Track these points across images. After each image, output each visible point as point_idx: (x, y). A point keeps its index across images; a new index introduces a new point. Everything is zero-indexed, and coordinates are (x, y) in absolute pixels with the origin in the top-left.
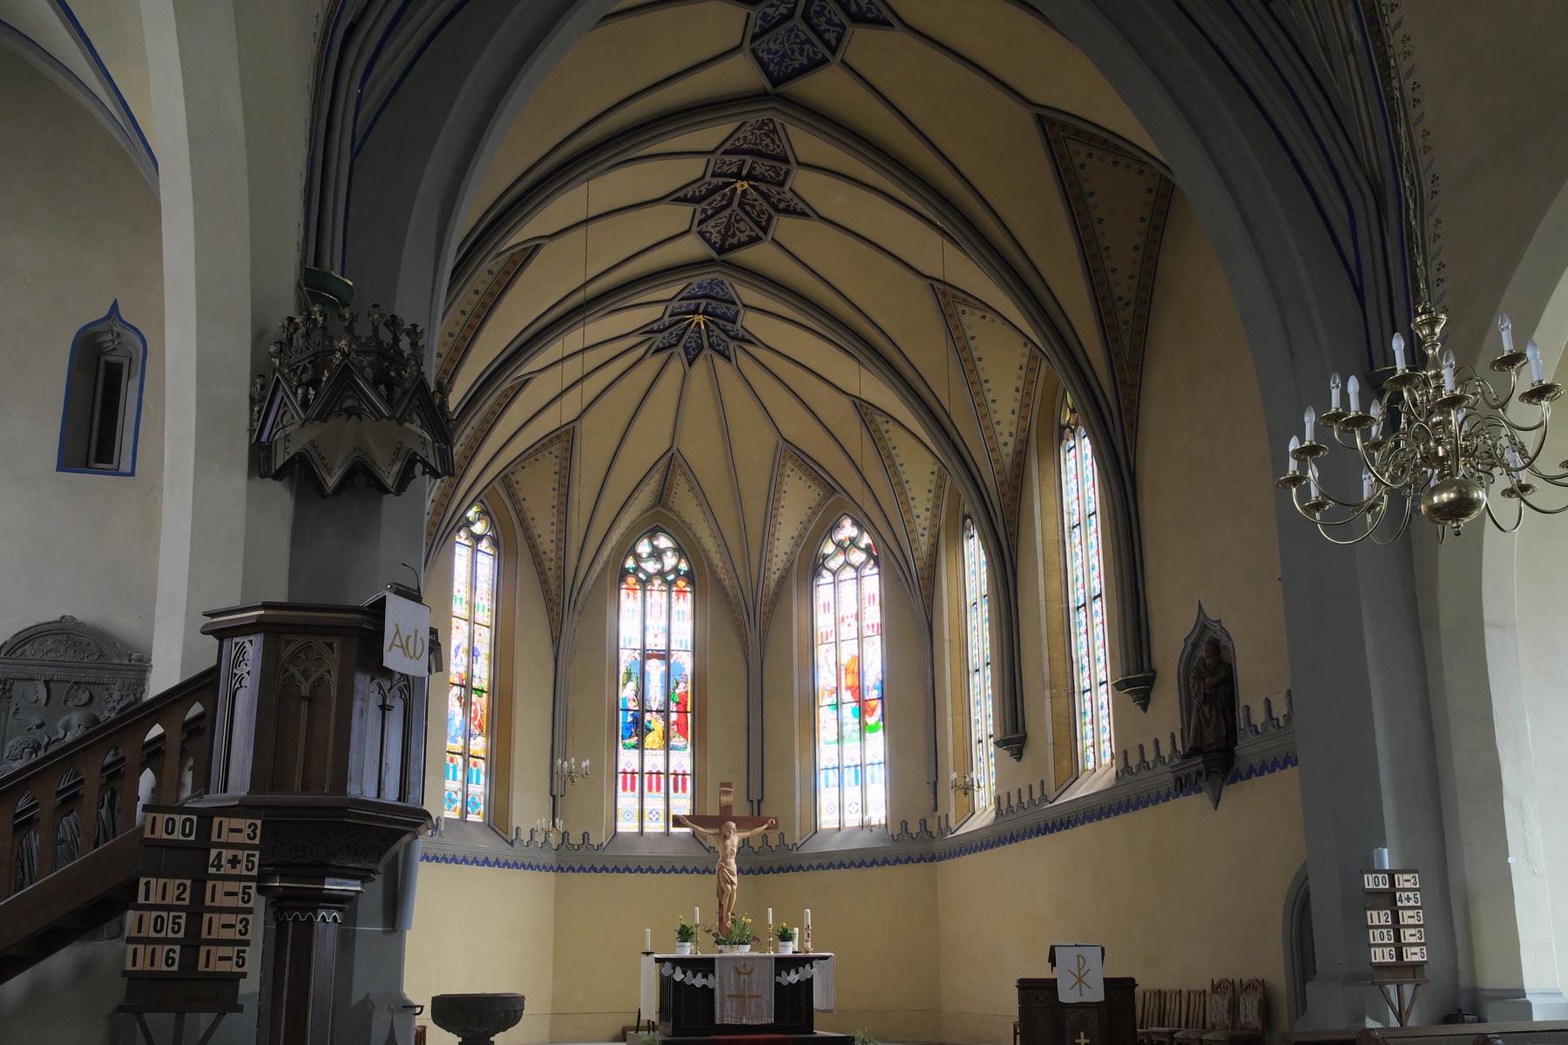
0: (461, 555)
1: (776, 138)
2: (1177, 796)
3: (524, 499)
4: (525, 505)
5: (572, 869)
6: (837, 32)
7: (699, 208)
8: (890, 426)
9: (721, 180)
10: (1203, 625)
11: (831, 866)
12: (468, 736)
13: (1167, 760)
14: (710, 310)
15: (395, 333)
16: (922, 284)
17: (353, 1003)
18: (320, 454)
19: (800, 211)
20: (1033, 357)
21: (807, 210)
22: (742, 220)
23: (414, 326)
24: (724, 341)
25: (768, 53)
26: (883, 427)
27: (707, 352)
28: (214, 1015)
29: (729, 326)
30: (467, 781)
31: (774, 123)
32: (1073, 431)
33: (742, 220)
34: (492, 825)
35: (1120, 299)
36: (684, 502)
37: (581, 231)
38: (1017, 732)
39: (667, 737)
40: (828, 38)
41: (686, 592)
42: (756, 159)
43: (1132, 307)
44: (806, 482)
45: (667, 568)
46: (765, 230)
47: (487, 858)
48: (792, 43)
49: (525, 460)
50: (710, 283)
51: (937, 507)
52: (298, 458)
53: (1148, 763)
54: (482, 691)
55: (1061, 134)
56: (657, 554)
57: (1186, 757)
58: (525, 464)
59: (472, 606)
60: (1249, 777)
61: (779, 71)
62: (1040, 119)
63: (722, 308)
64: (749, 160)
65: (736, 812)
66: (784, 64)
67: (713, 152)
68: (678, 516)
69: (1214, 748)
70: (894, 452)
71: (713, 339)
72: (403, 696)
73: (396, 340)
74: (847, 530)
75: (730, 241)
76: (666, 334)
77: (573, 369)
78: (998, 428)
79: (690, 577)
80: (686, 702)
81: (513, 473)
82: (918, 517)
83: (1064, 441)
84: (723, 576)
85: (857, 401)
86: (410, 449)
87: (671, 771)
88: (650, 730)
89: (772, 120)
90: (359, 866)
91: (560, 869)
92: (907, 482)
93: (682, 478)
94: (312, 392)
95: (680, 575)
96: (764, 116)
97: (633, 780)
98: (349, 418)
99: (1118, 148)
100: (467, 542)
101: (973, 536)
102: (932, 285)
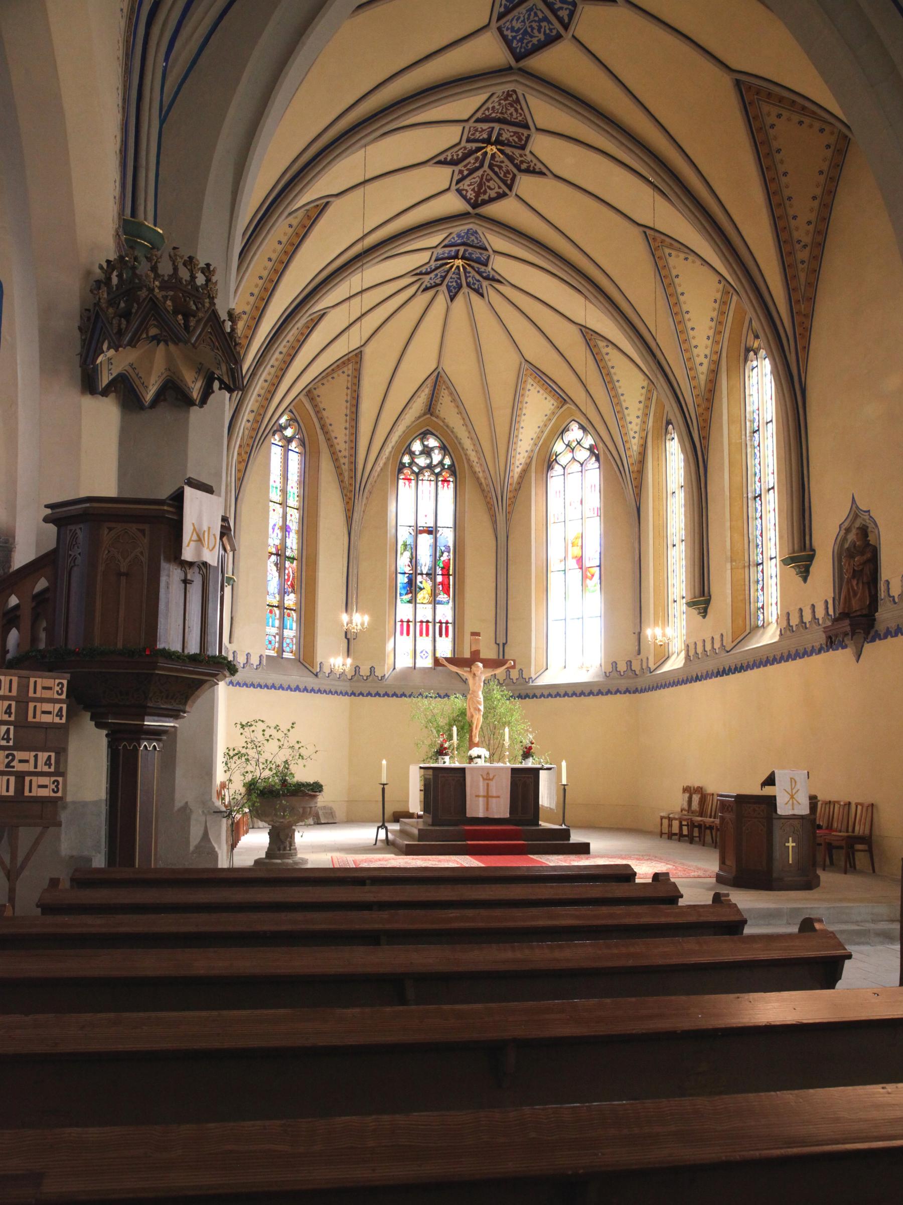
0: (276, 453)
1: (519, 107)
2: (828, 651)
3: (324, 409)
4: (325, 414)
5: (361, 694)
6: (570, 10)
7: (457, 169)
8: (610, 349)
9: (474, 146)
10: (855, 512)
11: (558, 695)
12: (283, 593)
13: (821, 622)
14: (467, 255)
15: (192, 271)
16: (636, 232)
17: (176, 808)
18: (137, 375)
19: (537, 171)
20: (725, 293)
21: (545, 170)
22: (491, 179)
23: (208, 265)
24: (478, 281)
25: (511, 32)
26: (604, 350)
27: (465, 289)
28: (38, 830)
29: (483, 268)
30: (282, 627)
31: (517, 95)
32: (756, 354)
33: (491, 179)
34: (301, 660)
35: (799, 242)
36: (446, 409)
37: (359, 192)
38: (704, 596)
39: (434, 594)
40: (561, 15)
41: (449, 481)
42: (503, 126)
43: (808, 249)
44: (543, 395)
45: (435, 462)
46: (510, 188)
47: (298, 686)
48: (532, 22)
49: (323, 378)
50: (467, 233)
51: (646, 415)
52: (120, 379)
53: (805, 623)
54: (294, 559)
55: (756, 97)
56: (427, 452)
57: (836, 620)
58: (325, 381)
59: (284, 492)
60: (885, 637)
61: (521, 47)
62: (738, 84)
63: (476, 254)
64: (497, 126)
65: (482, 656)
66: (525, 41)
67: (467, 121)
68: (443, 422)
69: (859, 613)
70: (612, 371)
71: (470, 279)
72: (201, 572)
73: (193, 277)
74: (575, 433)
75: (482, 197)
76: (432, 275)
77: (356, 307)
78: (695, 351)
79: (452, 469)
80: (449, 567)
81: (315, 389)
82: (630, 423)
83: (749, 362)
84: (478, 469)
85: (583, 329)
86: (209, 369)
87: (437, 620)
88: (421, 589)
89: (514, 91)
90: (170, 707)
91: (353, 694)
92: (622, 395)
93: (446, 391)
94: (124, 322)
95: (444, 468)
96: (509, 87)
97: (408, 626)
98: (158, 344)
99: (804, 108)
100: (280, 444)
101: (673, 439)
102: (645, 233)
